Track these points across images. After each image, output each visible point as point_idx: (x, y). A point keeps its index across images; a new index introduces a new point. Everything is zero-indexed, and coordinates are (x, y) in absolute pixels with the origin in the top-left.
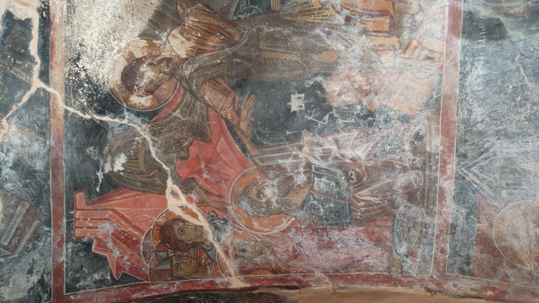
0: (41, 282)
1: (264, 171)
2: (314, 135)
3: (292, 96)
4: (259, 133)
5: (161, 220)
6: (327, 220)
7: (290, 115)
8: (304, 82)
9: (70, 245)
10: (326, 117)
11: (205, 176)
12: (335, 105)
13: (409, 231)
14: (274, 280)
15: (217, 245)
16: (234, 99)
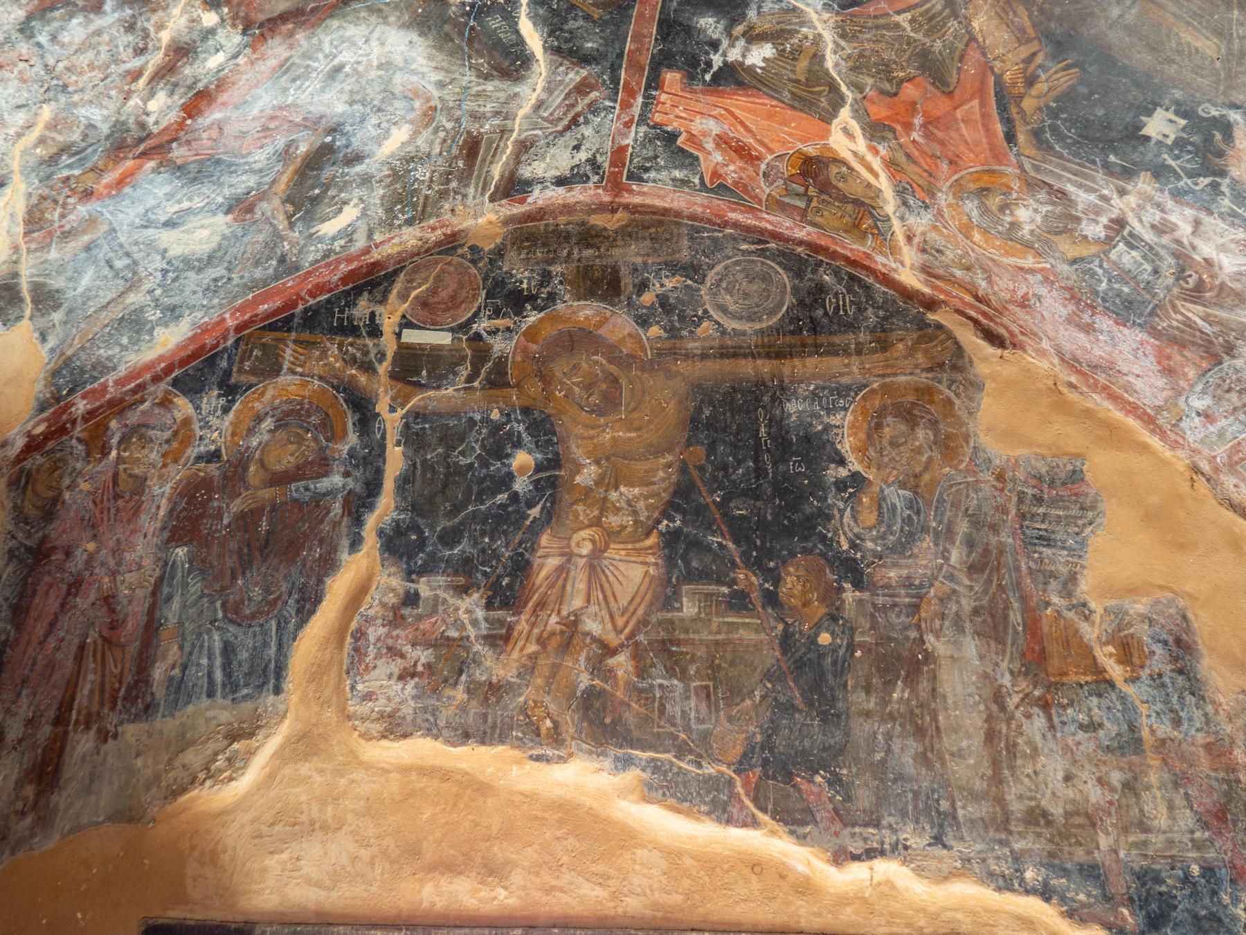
0: (592, 161)
1: (1031, 185)
2: (1162, 191)
3: (1159, 110)
4: (1054, 129)
5: (811, 151)
6: (1104, 300)
7: (1134, 135)
8: (1199, 103)
9: (643, 129)
10: (1204, 181)
11: (915, 135)
12: (1235, 172)
13: (1229, 391)
14: (972, 307)
15: (896, 223)
16: (1034, 55)
